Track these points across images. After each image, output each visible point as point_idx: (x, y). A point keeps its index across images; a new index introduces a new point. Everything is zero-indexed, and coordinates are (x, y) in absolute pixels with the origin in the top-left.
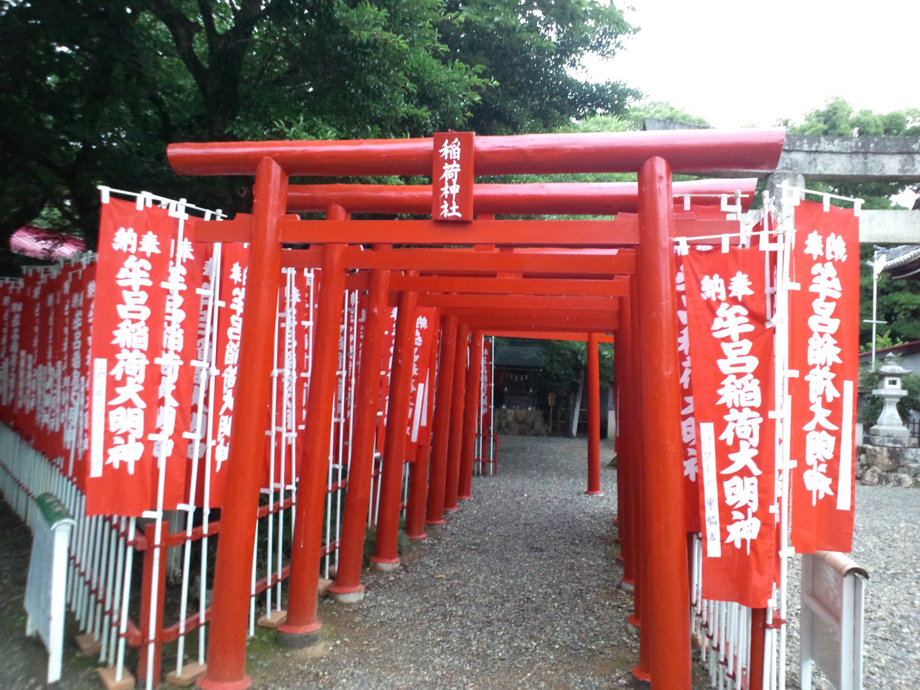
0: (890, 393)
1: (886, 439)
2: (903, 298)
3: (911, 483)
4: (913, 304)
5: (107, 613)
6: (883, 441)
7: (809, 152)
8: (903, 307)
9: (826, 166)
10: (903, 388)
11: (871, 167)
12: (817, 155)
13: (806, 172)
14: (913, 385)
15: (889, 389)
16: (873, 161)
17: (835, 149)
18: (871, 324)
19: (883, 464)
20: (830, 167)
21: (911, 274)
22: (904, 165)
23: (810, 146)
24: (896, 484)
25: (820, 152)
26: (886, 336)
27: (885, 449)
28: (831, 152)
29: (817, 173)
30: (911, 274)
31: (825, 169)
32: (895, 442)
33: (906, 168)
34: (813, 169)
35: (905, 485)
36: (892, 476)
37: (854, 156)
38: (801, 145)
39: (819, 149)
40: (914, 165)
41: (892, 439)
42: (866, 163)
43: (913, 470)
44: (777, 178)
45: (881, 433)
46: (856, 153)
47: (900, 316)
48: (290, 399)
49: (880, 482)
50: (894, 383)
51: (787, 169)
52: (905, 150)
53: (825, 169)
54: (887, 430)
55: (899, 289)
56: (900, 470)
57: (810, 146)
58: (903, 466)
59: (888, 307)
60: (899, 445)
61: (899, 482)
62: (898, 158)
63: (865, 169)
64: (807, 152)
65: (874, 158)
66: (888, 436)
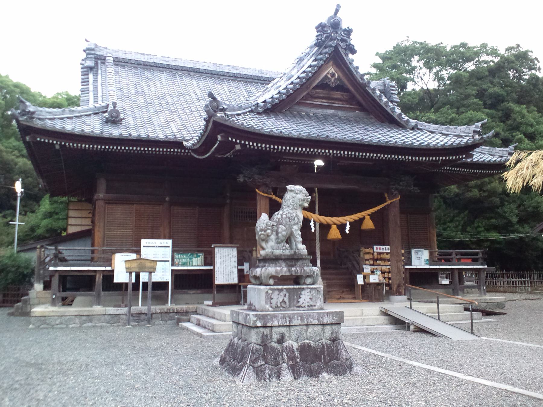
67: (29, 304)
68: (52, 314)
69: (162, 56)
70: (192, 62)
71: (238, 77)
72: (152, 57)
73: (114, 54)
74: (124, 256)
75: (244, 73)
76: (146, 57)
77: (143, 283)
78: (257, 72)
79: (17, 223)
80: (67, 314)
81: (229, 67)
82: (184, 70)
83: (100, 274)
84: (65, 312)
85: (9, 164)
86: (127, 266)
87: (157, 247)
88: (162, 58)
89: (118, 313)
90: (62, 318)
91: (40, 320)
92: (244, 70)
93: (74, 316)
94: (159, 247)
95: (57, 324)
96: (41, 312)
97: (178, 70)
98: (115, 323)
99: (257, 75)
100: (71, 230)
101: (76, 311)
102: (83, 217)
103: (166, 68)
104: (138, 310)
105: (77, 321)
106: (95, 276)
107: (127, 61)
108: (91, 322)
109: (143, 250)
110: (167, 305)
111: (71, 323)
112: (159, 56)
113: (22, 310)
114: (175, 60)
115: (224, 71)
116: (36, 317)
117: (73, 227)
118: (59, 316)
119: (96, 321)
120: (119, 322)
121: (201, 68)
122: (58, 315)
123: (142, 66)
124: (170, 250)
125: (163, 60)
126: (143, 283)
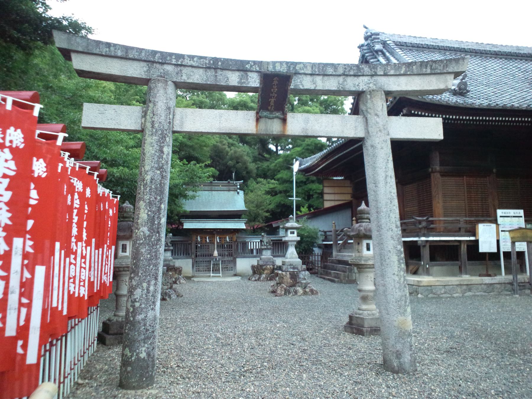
0: (291, 239)
1: (289, 267)
2: (314, 186)
3: (302, 293)
4: (319, 190)
5: (42, 356)
6: (288, 268)
7: (176, 65)
8: (314, 191)
9: (189, 77)
10: (298, 236)
11: (220, 79)
12: (182, 68)
13: (175, 80)
14: (313, 234)
15: (290, 237)
16: (221, 74)
17: (194, 64)
18: (293, 200)
19: (287, 282)
20: (192, 77)
21: (313, 172)
22: (241, 79)
23: (177, 61)
24: (294, 294)
25: (185, 66)
26: (305, 207)
27: (288, 273)
28: (192, 66)
29: (182, 81)
30: (313, 172)
31: (188, 79)
32: (294, 268)
33: (242, 81)
34: (179, 78)
35: (299, 294)
36: (292, 289)
37: (208, 70)
38: (171, 60)
39: (183, 63)
40: (247, 79)
41: (292, 266)
42: (216, 76)
43: (303, 284)
44: (153, 83)
45: (287, 264)
46: (209, 68)
47: (315, 196)
48: (505, 213)
49: (285, 294)
50: (293, 233)
51: (161, 76)
52: (241, 68)
53: (188, 79)
54: (290, 261)
55: (313, 182)
56: (297, 285)
57: (177, 61)
58: (298, 283)
59: (307, 191)
60: (296, 270)
61: (296, 292)
62: (237, 74)
63: (216, 80)
64: (175, 65)
65: (221, 73)
66: (290, 265)
67: (354, 272)
68: (437, 284)
69: (431, 38)
70: (457, 42)
71: (499, 55)
72: (423, 39)
73: (391, 38)
74: (486, 227)
75: (503, 50)
76: (418, 39)
77: (504, 253)
78: (515, 48)
79: (294, 198)
80: (450, 284)
81: (490, 46)
82: (452, 50)
83: (465, 245)
84: (448, 281)
85: (222, 152)
86: (512, 236)
87: (511, 217)
88: (431, 40)
89: (493, 282)
90: (446, 287)
91: (427, 290)
92: (503, 48)
93: (455, 285)
94: (514, 217)
95: (442, 294)
96: (429, 282)
97: (447, 50)
98: (491, 292)
99: (515, 51)
100: (327, 205)
101: (457, 280)
102: (336, 193)
103: (436, 49)
104: (509, 280)
105: (459, 290)
106: (460, 245)
107: (404, 44)
108: (470, 291)
109: (500, 220)
110: (524, 274)
111: (455, 292)
112: (429, 38)
113: (348, 278)
114: (443, 41)
115: (486, 49)
116: (423, 286)
117: (329, 202)
118: (443, 285)
119: (475, 291)
120: (494, 292)
121: (466, 47)
122: (443, 284)
123: (416, 48)
124: (522, 219)
125: (433, 42)
126: (504, 253)
